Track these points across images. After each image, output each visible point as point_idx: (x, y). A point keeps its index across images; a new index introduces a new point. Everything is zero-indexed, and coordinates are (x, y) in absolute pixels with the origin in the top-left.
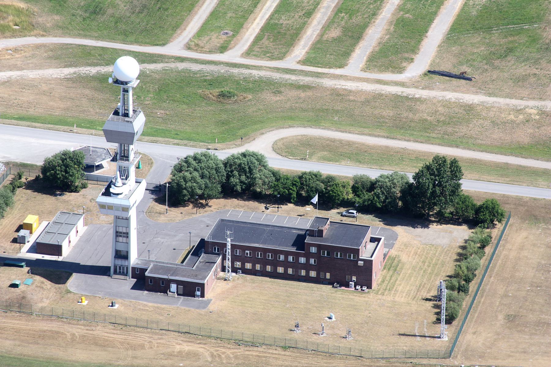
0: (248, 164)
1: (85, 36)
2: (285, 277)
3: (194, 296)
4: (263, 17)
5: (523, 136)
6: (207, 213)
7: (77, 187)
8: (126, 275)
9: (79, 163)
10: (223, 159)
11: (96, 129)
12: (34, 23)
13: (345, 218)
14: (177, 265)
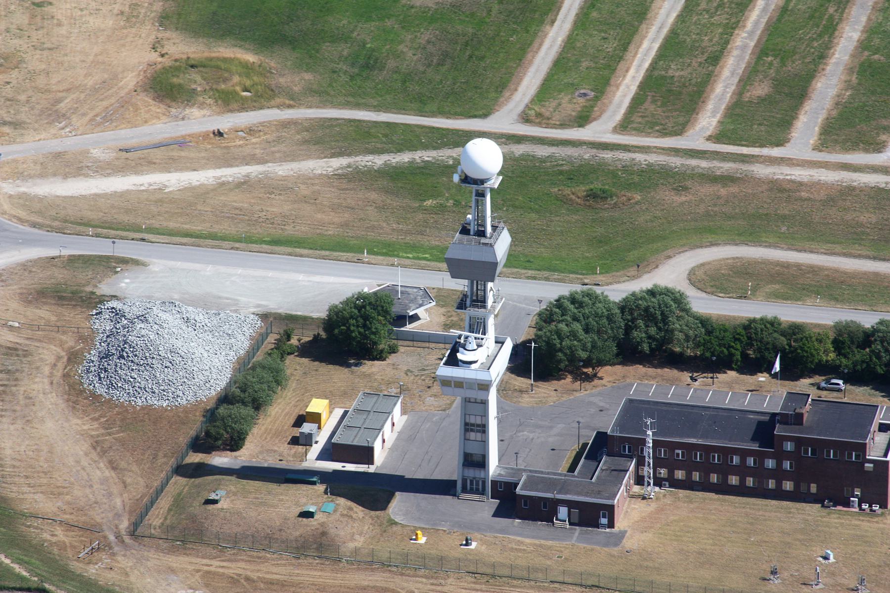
0: (660, 307)
1: (358, 106)
2: (741, 491)
3: (597, 525)
4: (640, 66)
6: (598, 389)
7: (382, 351)
8: (483, 492)
9: (386, 313)
10: (617, 301)
11: (398, 256)
12: (273, 87)
13: (825, 393)
14: (560, 475)
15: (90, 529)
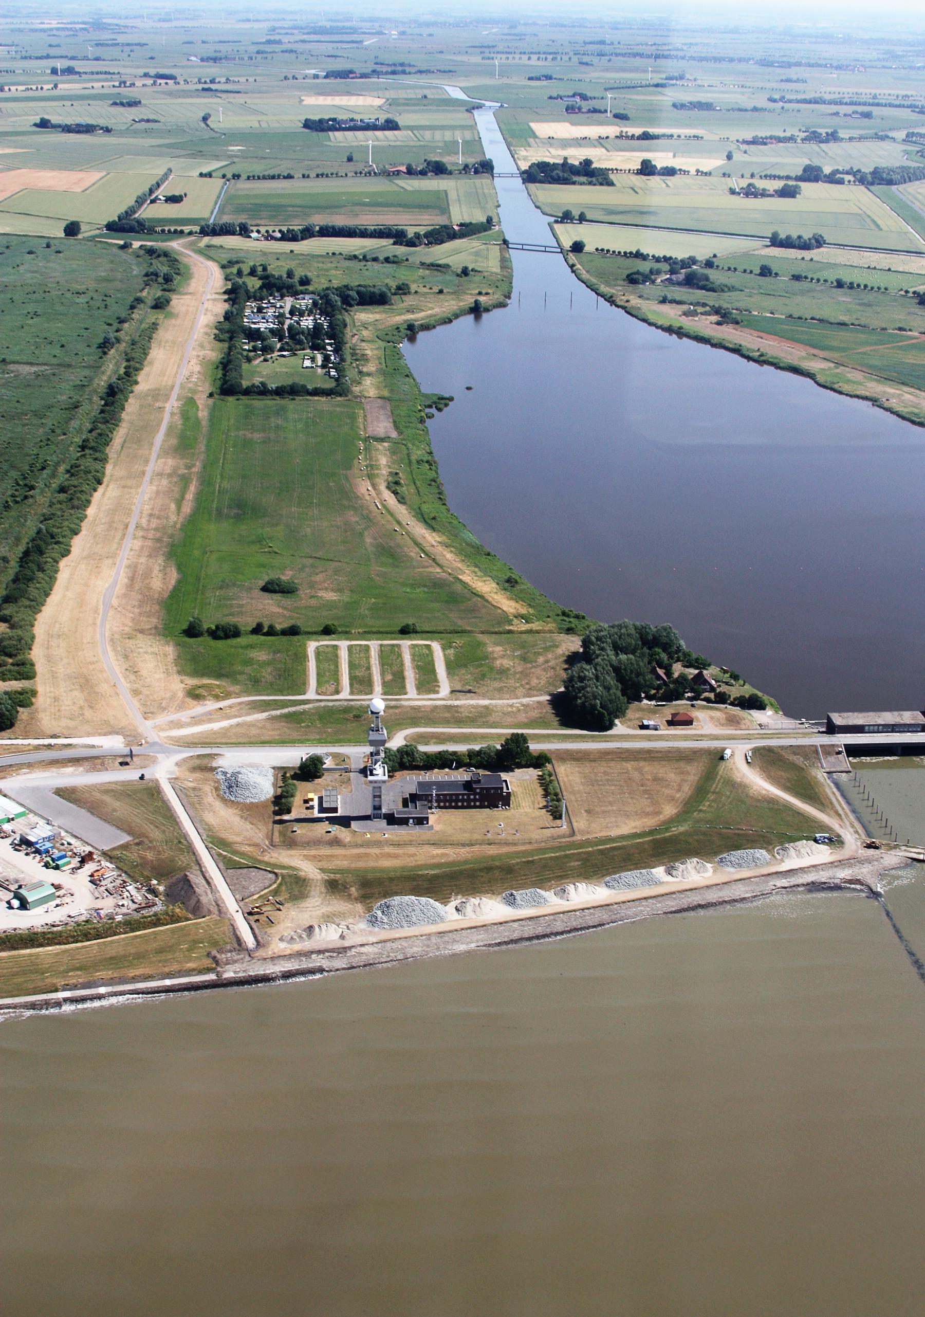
2: (463, 807)
3: (423, 824)
5: (522, 717)
15: (256, 845)
